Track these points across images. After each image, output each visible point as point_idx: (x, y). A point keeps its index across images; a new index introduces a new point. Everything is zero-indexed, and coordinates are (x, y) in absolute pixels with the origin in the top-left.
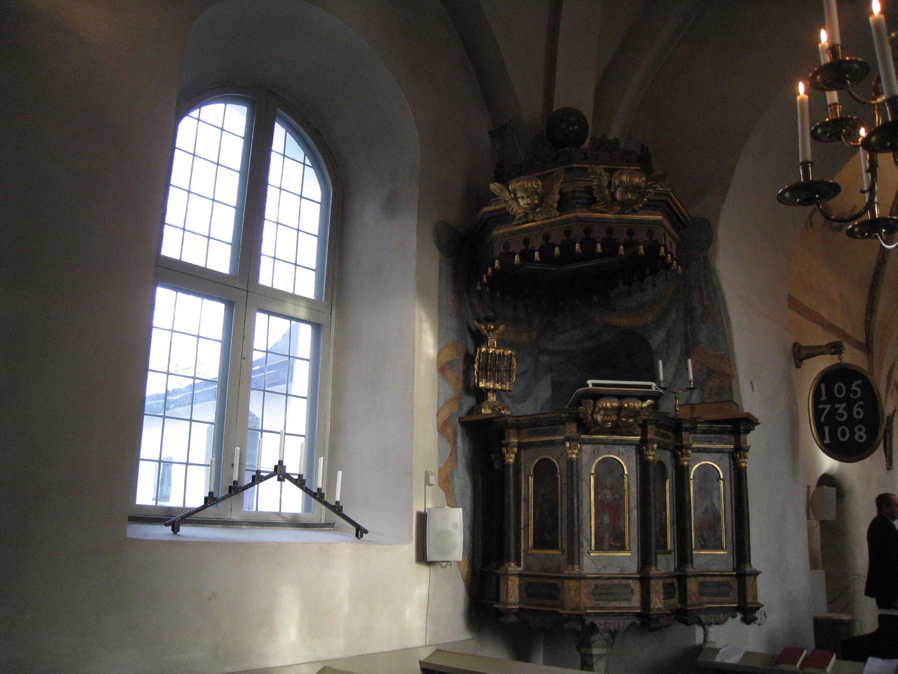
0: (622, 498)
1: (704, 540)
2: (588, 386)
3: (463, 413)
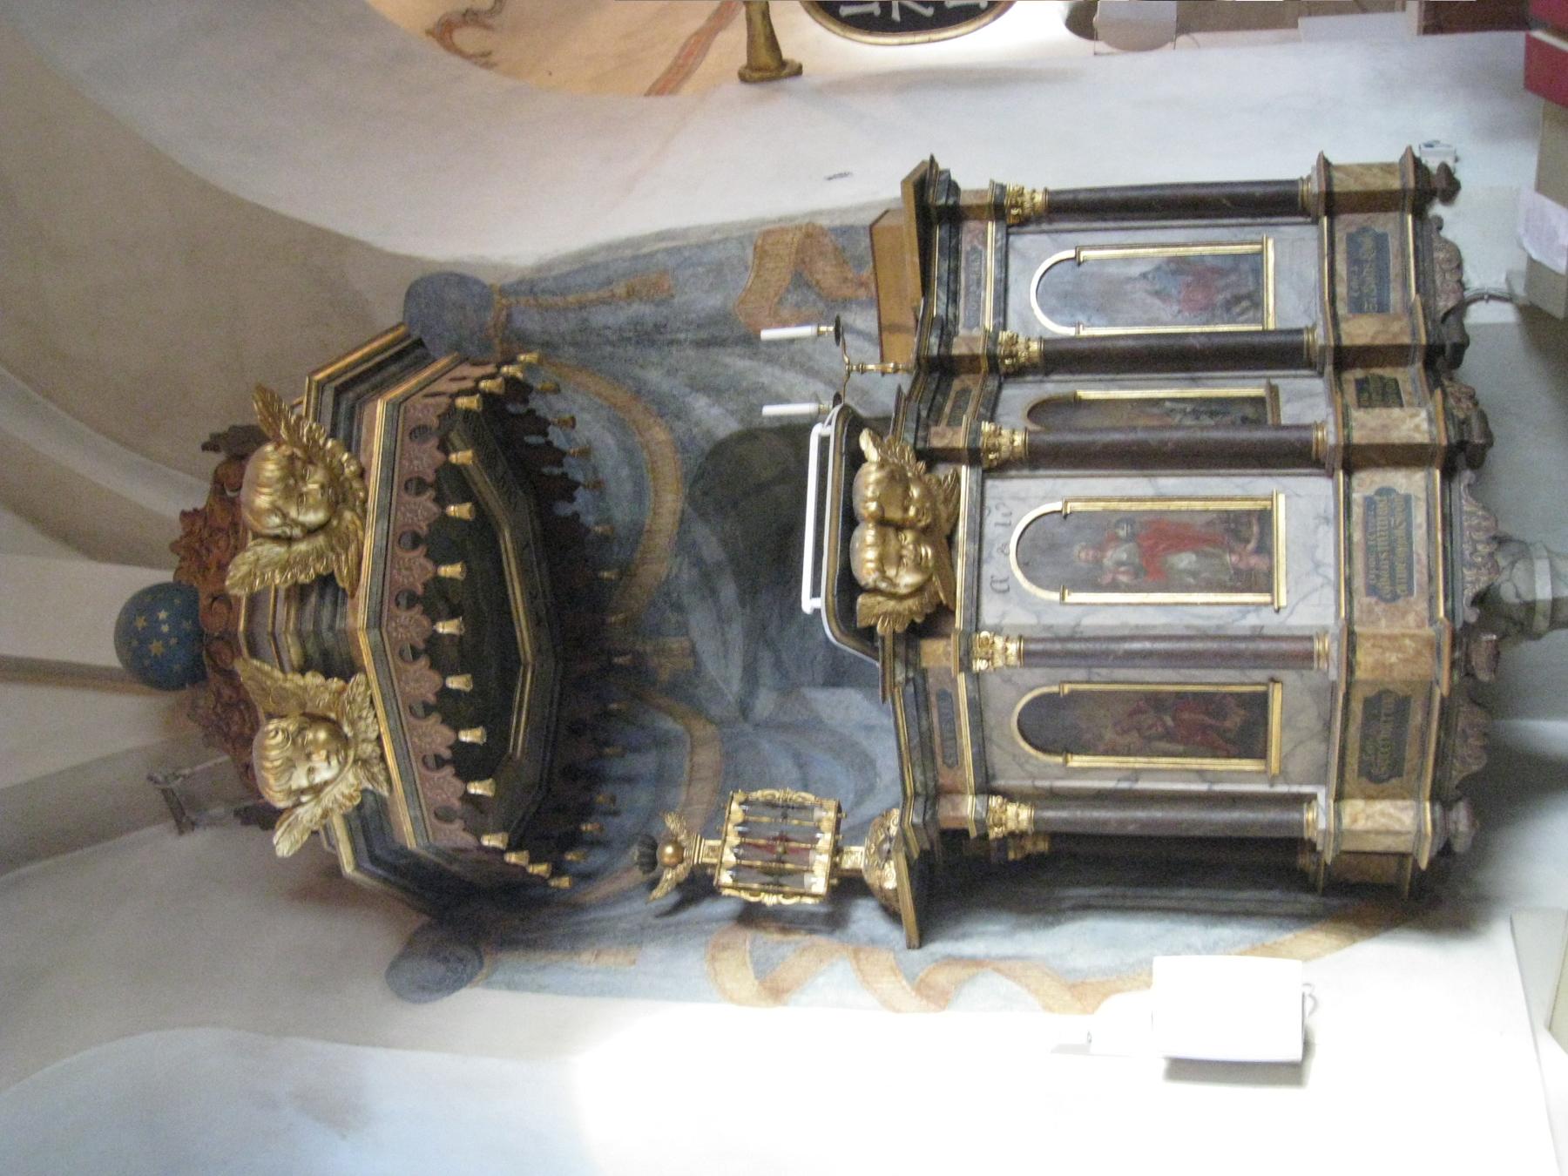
0: (1129, 518)
1: (1237, 299)
2: (817, 612)
3: (897, 937)
